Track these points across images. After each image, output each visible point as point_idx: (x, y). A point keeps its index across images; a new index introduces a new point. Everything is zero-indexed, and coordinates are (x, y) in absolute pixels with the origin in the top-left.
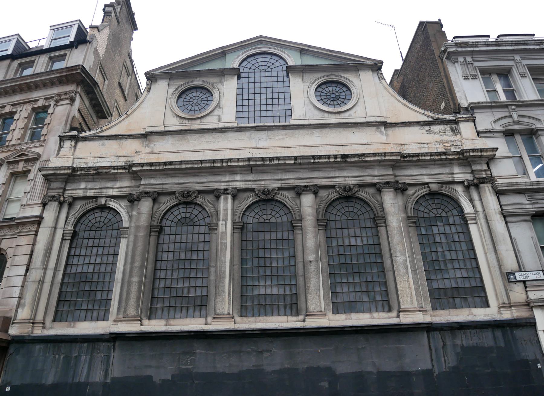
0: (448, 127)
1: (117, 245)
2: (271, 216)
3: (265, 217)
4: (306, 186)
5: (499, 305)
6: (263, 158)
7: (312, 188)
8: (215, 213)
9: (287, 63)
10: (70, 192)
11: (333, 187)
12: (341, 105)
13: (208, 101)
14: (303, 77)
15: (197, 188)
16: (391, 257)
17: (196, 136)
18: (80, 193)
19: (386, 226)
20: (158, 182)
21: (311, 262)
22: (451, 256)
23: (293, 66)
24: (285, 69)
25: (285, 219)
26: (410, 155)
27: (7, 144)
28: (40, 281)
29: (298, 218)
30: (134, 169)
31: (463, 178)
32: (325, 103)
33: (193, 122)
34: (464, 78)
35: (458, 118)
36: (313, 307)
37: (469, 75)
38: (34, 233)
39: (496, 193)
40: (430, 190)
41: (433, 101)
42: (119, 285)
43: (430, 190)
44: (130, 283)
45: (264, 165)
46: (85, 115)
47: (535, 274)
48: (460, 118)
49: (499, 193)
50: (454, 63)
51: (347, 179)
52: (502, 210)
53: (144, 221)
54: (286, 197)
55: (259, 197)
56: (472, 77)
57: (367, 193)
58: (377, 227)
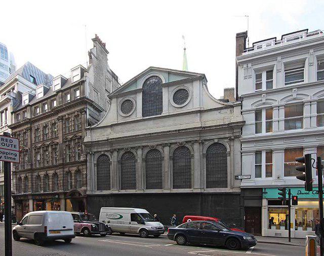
0: (229, 110)
33: (126, 119)
36: (166, 187)
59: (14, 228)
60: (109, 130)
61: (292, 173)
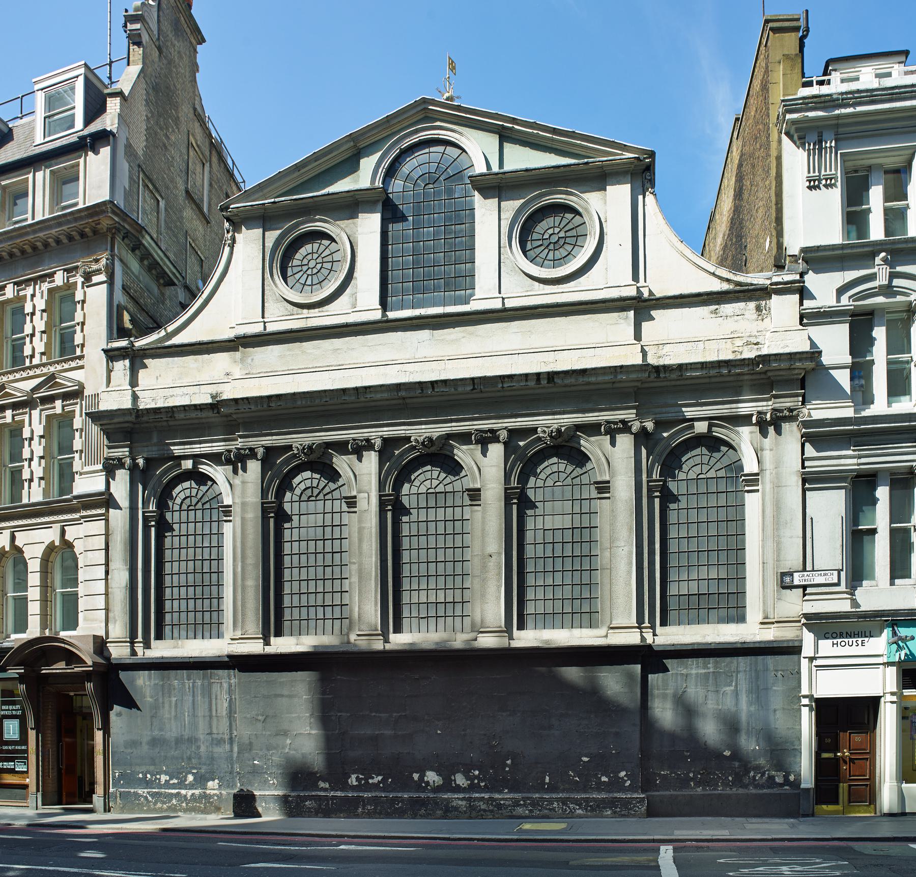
1: (220, 534)
13: (333, 262)
27: (27, 364)
42: (231, 589)
46: (136, 292)
47: (825, 575)
59: (151, 700)
60: (222, 360)
61: (797, 727)
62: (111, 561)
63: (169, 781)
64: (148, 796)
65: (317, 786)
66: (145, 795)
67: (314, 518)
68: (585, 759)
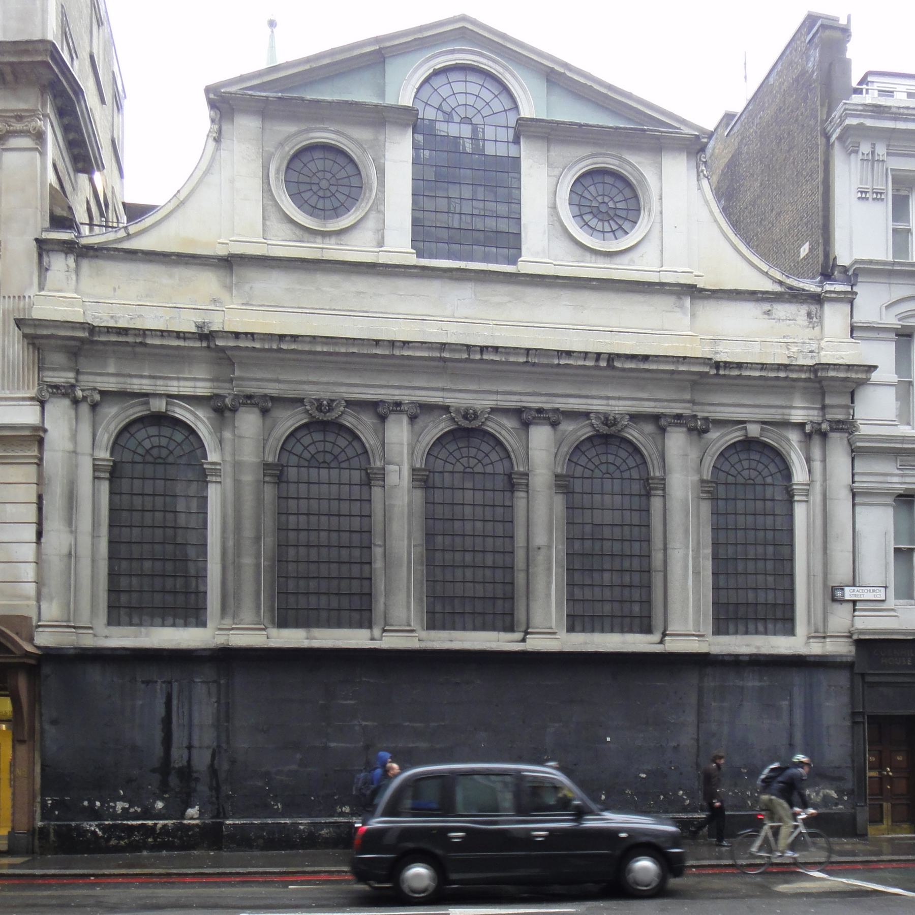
0: (803, 309)
2: (464, 459)
3: (464, 461)
4: (540, 411)
5: (810, 634)
6: (468, 346)
7: (550, 415)
8: (380, 447)
9: (516, 107)
10: (91, 378)
11: (586, 415)
12: (617, 233)
14: (548, 151)
15: (345, 395)
16: (665, 549)
17: (335, 278)
18: (110, 384)
19: (664, 496)
20: (269, 376)
21: (539, 548)
22: (622, 516)
23: (532, 120)
24: (512, 123)
25: (499, 468)
26: (727, 365)
28: (70, 554)
29: (521, 469)
30: (220, 343)
31: (806, 418)
32: (581, 216)
33: (319, 243)
34: (859, 195)
35: (826, 292)
36: (538, 618)
37: (870, 190)
38: (36, 461)
39: (852, 451)
40: (746, 436)
41: (789, 231)
43: (746, 436)
44: (238, 567)
45: (468, 360)
47: (874, 591)
48: (831, 292)
49: (855, 453)
50: (850, 154)
51: (611, 402)
52: (853, 482)
53: (249, 455)
54: (502, 426)
55: (457, 423)
56: (875, 196)
57: (641, 433)
58: (648, 495)
62: (47, 519)
63: (128, 809)
64: (97, 830)
65: (335, 811)
66: (93, 829)
67: (348, 490)
68: (644, 776)
